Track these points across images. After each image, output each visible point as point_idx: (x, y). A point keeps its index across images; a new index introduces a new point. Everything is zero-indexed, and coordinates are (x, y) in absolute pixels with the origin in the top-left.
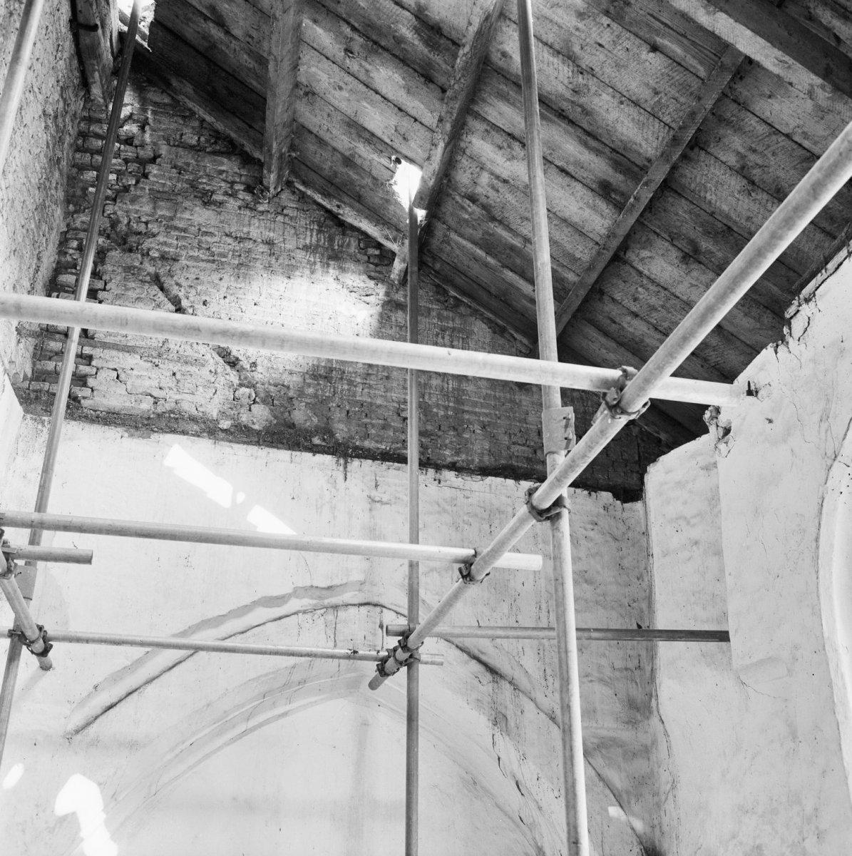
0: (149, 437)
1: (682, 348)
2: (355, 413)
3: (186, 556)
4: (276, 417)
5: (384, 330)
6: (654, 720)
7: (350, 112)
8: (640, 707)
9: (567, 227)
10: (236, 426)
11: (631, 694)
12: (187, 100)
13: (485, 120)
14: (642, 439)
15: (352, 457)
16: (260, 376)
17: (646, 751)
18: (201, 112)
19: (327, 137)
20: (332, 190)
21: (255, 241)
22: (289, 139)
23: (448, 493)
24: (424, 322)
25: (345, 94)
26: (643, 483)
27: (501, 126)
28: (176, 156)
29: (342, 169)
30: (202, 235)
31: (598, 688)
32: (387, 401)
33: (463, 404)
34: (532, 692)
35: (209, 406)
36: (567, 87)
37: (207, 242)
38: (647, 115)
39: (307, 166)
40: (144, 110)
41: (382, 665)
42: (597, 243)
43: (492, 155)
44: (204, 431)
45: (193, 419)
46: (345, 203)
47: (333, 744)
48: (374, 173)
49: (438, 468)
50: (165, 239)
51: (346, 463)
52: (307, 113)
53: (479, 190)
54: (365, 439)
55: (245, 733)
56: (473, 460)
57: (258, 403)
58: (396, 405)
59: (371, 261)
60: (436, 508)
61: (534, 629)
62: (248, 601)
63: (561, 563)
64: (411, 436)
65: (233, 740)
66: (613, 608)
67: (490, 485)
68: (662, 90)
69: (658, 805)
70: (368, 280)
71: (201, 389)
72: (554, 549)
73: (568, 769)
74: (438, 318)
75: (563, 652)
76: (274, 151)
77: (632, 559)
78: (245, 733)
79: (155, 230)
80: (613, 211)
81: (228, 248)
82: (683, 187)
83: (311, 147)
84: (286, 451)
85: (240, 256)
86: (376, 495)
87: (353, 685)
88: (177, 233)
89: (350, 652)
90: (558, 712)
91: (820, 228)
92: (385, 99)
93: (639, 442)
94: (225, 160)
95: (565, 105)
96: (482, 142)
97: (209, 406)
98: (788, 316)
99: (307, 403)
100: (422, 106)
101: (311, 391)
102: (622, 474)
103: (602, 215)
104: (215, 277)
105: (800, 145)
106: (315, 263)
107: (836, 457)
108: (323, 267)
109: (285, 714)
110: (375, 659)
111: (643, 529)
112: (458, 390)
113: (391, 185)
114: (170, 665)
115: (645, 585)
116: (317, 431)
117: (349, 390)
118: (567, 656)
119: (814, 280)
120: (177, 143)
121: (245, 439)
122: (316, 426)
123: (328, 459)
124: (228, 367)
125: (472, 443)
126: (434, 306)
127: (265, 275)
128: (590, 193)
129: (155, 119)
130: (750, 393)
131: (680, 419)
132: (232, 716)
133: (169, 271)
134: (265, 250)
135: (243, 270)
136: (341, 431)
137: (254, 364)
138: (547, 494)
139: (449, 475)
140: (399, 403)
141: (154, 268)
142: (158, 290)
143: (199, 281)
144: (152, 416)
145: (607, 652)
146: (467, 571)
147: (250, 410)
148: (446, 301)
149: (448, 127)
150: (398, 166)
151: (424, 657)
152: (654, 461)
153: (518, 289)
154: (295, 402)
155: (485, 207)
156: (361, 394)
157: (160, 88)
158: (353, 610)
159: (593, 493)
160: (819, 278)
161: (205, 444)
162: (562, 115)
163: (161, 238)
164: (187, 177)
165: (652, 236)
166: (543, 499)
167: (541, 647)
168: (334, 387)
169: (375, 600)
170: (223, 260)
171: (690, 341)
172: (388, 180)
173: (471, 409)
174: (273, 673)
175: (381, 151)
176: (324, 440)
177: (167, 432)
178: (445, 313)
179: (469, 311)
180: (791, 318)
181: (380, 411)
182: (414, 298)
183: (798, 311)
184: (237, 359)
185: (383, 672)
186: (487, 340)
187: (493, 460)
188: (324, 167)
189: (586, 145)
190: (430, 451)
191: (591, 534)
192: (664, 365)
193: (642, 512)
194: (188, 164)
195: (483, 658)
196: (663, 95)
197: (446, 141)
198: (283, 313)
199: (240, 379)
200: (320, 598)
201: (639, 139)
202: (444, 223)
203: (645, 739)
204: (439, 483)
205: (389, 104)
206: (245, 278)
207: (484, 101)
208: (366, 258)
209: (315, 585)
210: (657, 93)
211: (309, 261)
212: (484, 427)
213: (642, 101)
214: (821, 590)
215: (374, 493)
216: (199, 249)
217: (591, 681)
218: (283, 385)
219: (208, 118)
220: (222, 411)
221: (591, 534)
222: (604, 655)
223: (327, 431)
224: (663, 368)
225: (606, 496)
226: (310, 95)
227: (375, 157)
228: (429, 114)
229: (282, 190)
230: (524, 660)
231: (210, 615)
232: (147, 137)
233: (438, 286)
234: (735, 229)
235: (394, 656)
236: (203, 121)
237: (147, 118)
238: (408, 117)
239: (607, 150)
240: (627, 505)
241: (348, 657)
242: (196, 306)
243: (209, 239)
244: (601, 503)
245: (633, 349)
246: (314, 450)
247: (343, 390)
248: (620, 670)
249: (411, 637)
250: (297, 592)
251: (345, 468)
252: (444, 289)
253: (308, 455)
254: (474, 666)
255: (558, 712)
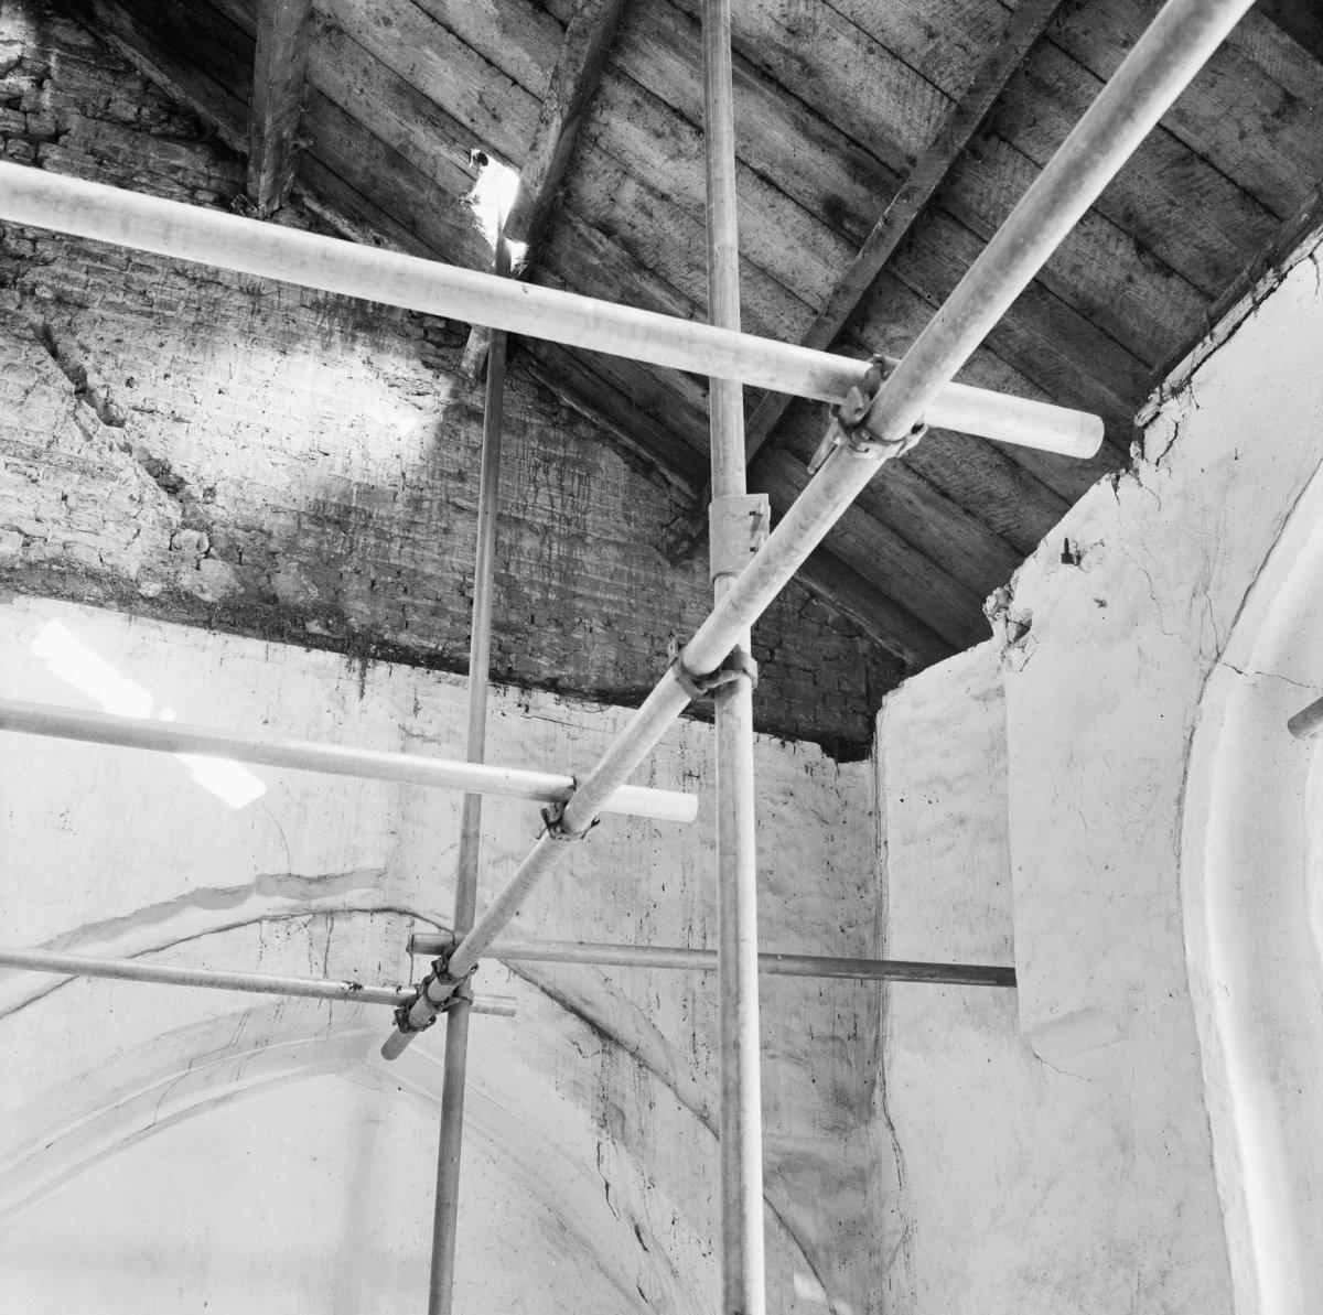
0: (11, 602)
1: (1006, 274)
2: (386, 585)
3: (63, 811)
4: (244, 583)
5: (444, 453)
6: (879, 1125)
7: (402, 67)
8: (854, 1100)
9: (766, 281)
10: (170, 593)
11: (839, 1080)
12: (120, 43)
13: (634, 83)
14: (874, 661)
15: (374, 657)
16: (220, 511)
17: (861, 1179)
18: (145, 66)
19: (359, 112)
20: (366, 210)
21: (227, 288)
22: (295, 116)
23: (541, 728)
24: (513, 445)
25: (395, 32)
26: (871, 725)
27: (662, 95)
28: (97, 135)
29: (384, 172)
30: (133, 270)
31: (784, 1068)
32: (442, 569)
33: (575, 584)
34: (671, 1074)
35: (124, 557)
36: (778, 23)
37: (142, 283)
38: (913, 76)
39: (325, 166)
40: (45, 54)
41: (405, 1011)
42: (815, 312)
43: (643, 149)
44: (112, 598)
45: (93, 576)
46: (388, 235)
47: (313, 1148)
48: (441, 180)
49: (525, 686)
50: (66, 270)
51: (364, 668)
52: (329, 69)
53: (619, 212)
54: (401, 630)
55: (151, 1129)
56: (587, 677)
57: (213, 557)
58: (459, 577)
59: (430, 337)
60: (520, 753)
61: (678, 951)
62: (169, 894)
63: (734, 774)
64: (479, 616)
65: (127, 1142)
66: (814, 935)
67: (615, 720)
68: (941, 29)
69: (879, 1271)
70: (422, 369)
71: (111, 526)
72: (721, 750)
73: (731, 1165)
74: (540, 440)
75: (733, 997)
76: (267, 131)
77: (850, 853)
78: (151, 1129)
79: (49, 254)
80: (846, 253)
81: (177, 294)
82: (968, 212)
83: (334, 131)
84: (259, 642)
85: (198, 309)
86: (416, 725)
87: (358, 1049)
88: (88, 262)
89: (347, 986)
90: (715, 1109)
91: (1195, 286)
92: (464, 42)
93: (869, 664)
94: (184, 150)
95: (774, 58)
96: (627, 124)
97: (124, 557)
98: (1139, 423)
99: (301, 563)
100: (527, 58)
101: (310, 542)
102: (839, 715)
103: (827, 261)
104: (152, 340)
105: (1172, 134)
106: (331, 332)
107: (1219, 655)
108: (344, 340)
109: (226, 1099)
110: (391, 1000)
111: (870, 806)
112: (568, 559)
113: (468, 202)
114: (20, 1003)
115: (868, 899)
116: (317, 611)
117: (377, 546)
118: (738, 952)
119: (1191, 355)
120: (99, 114)
121: (186, 617)
122: (315, 603)
123: (333, 658)
124: (164, 495)
125: (587, 649)
126: (534, 421)
127: (240, 345)
128: (807, 221)
129: (62, 71)
130: (1067, 558)
131: (938, 626)
132: (129, 1097)
133: (69, 324)
134: (245, 304)
135: (202, 334)
136: (359, 611)
137: (211, 492)
138: (713, 639)
139: (545, 699)
140: (463, 574)
141: (42, 317)
142: (46, 353)
143: (121, 346)
144: (18, 566)
145: (802, 1010)
146: (557, 816)
147: (198, 568)
148: (556, 414)
149: (570, 88)
150: (482, 168)
151: (478, 1001)
152: (895, 686)
153: (679, 394)
154: (279, 559)
155: (628, 245)
156: (399, 555)
157: (75, 21)
158: (361, 920)
159: (788, 743)
160: (1199, 351)
161: (111, 621)
162: (766, 74)
163: (58, 269)
164: (112, 171)
165: (910, 301)
166: (703, 652)
167: (690, 997)
168: (352, 540)
169: (403, 903)
170: (168, 313)
171: (1025, 254)
172: (464, 194)
173: (587, 592)
174: (207, 1023)
175: (454, 140)
176: (328, 627)
177: (41, 595)
178: (552, 433)
179: (593, 432)
180: (1146, 426)
181: (430, 586)
182: (497, 405)
183: (1158, 414)
184: (181, 480)
185: (406, 1023)
186: (622, 482)
187: (622, 678)
188: (355, 167)
189: (804, 130)
190: (513, 657)
191: (784, 810)
192: (966, 318)
193: (869, 785)
194: (117, 151)
195: (588, 1011)
196: (942, 38)
197: (565, 114)
198: (269, 410)
199: (184, 515)
200: (304, 896)
201: (896, 121)
202: (556, 273)
203: (857, 1157)
204: (527, 710)
205: (471, 51)
206: (204, 347)
207: (635, 48)
208: (420, 332)
209: (296, 872)
210: (931, 36)
211: (320, 329)
212: (608, 624)
213: (906, 50)
214: (1185, 889)
215: (410, 722)
216: (126, 293)
217: (773, 1056)
218: (261, 531)
219: (159, 78)
220: (148, 565)
221: (784, 810)
222: (797, 1013)
223: (333, 611)
224: (962, 327)
225: (813, 749)
226: (334, 32)
227: (443, 150)
228: (539, 72)
229: (281, 208)
230: (654, 1006)
231: (100, 916)
232: (46, 99)
233: (542, 388)
234: (1051, 287)
235: (426, 992)
236: (148, 82)
237: (49, 68)
238: (502, 77)
239: (841, 141)
240: (844, 766)
241: (344, 996)
242: (113, 387)
243: (146, 277)
244: (802, 761)
245: (868, 502)
246: (309, 642)
247: (366, 546)
248: (823, 1039)
249: (456, 955)
250: (262, 884)
251: (363, 675)
252: (553, 395)
253: (296, 651)
254: (572, 1024)
255: (715, 1109)
